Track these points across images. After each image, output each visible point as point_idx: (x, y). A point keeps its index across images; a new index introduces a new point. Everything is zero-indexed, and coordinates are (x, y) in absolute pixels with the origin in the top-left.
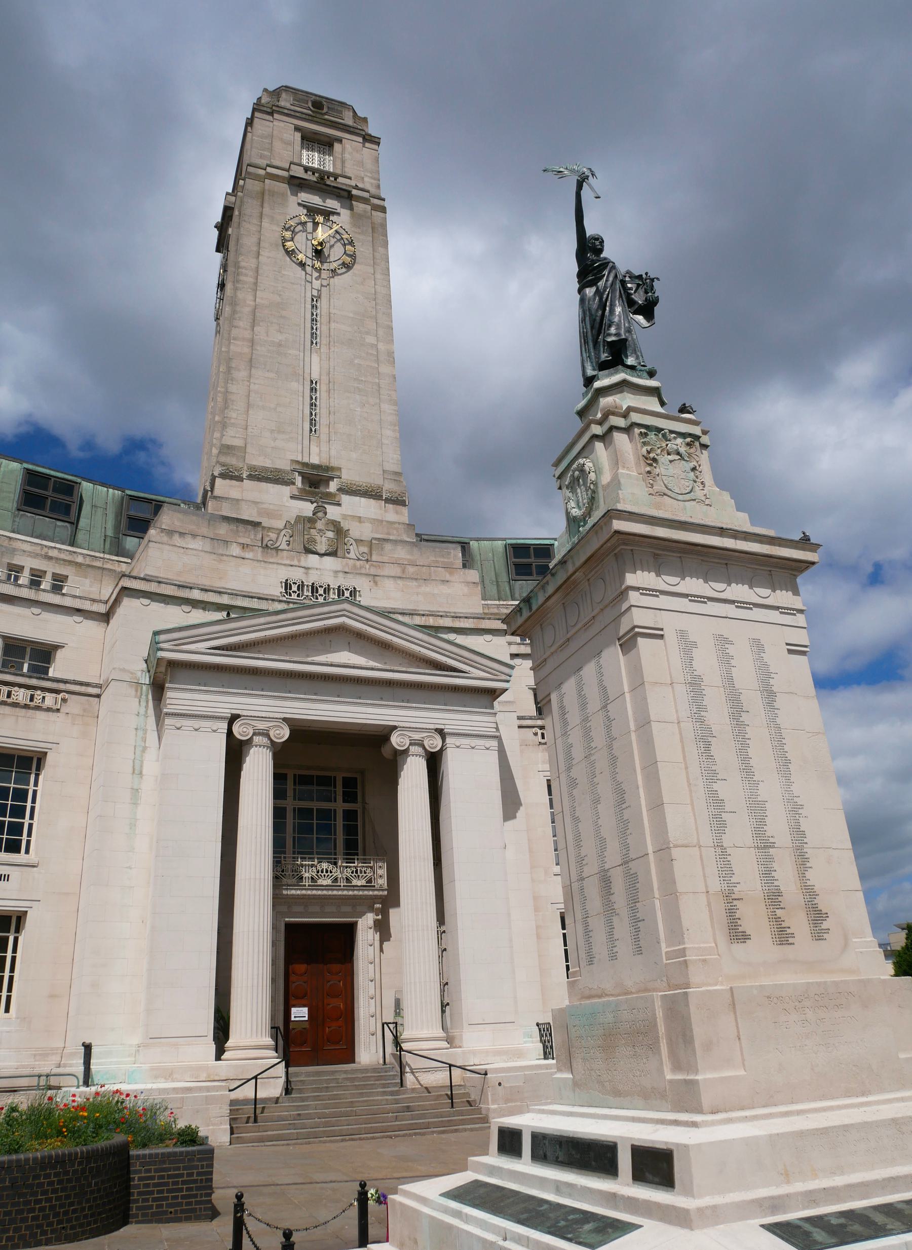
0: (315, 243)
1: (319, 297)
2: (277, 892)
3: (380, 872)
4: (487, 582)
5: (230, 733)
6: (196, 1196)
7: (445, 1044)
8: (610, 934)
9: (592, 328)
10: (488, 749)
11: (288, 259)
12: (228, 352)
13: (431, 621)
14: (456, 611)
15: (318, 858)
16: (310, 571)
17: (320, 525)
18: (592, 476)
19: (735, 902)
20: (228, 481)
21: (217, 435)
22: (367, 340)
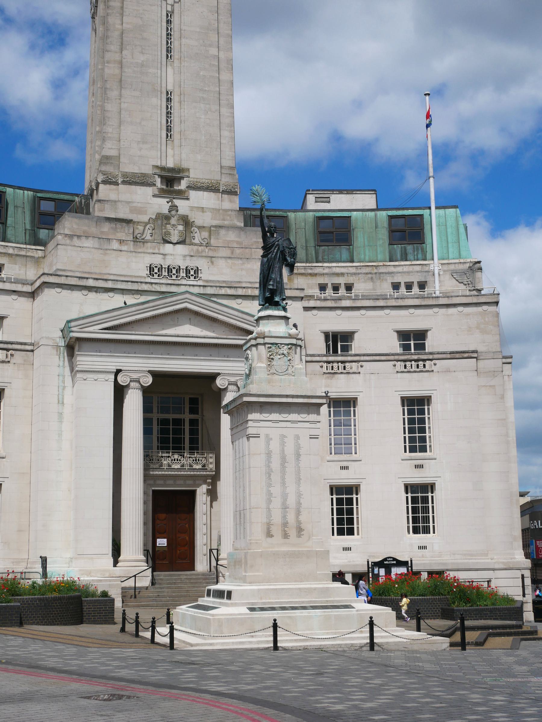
2: (147, 472)
3: (211, 460)
6: (108, 615)
15: (172, 452)
16: (167, 257)
17: (173, 221)
20: (108, 186)
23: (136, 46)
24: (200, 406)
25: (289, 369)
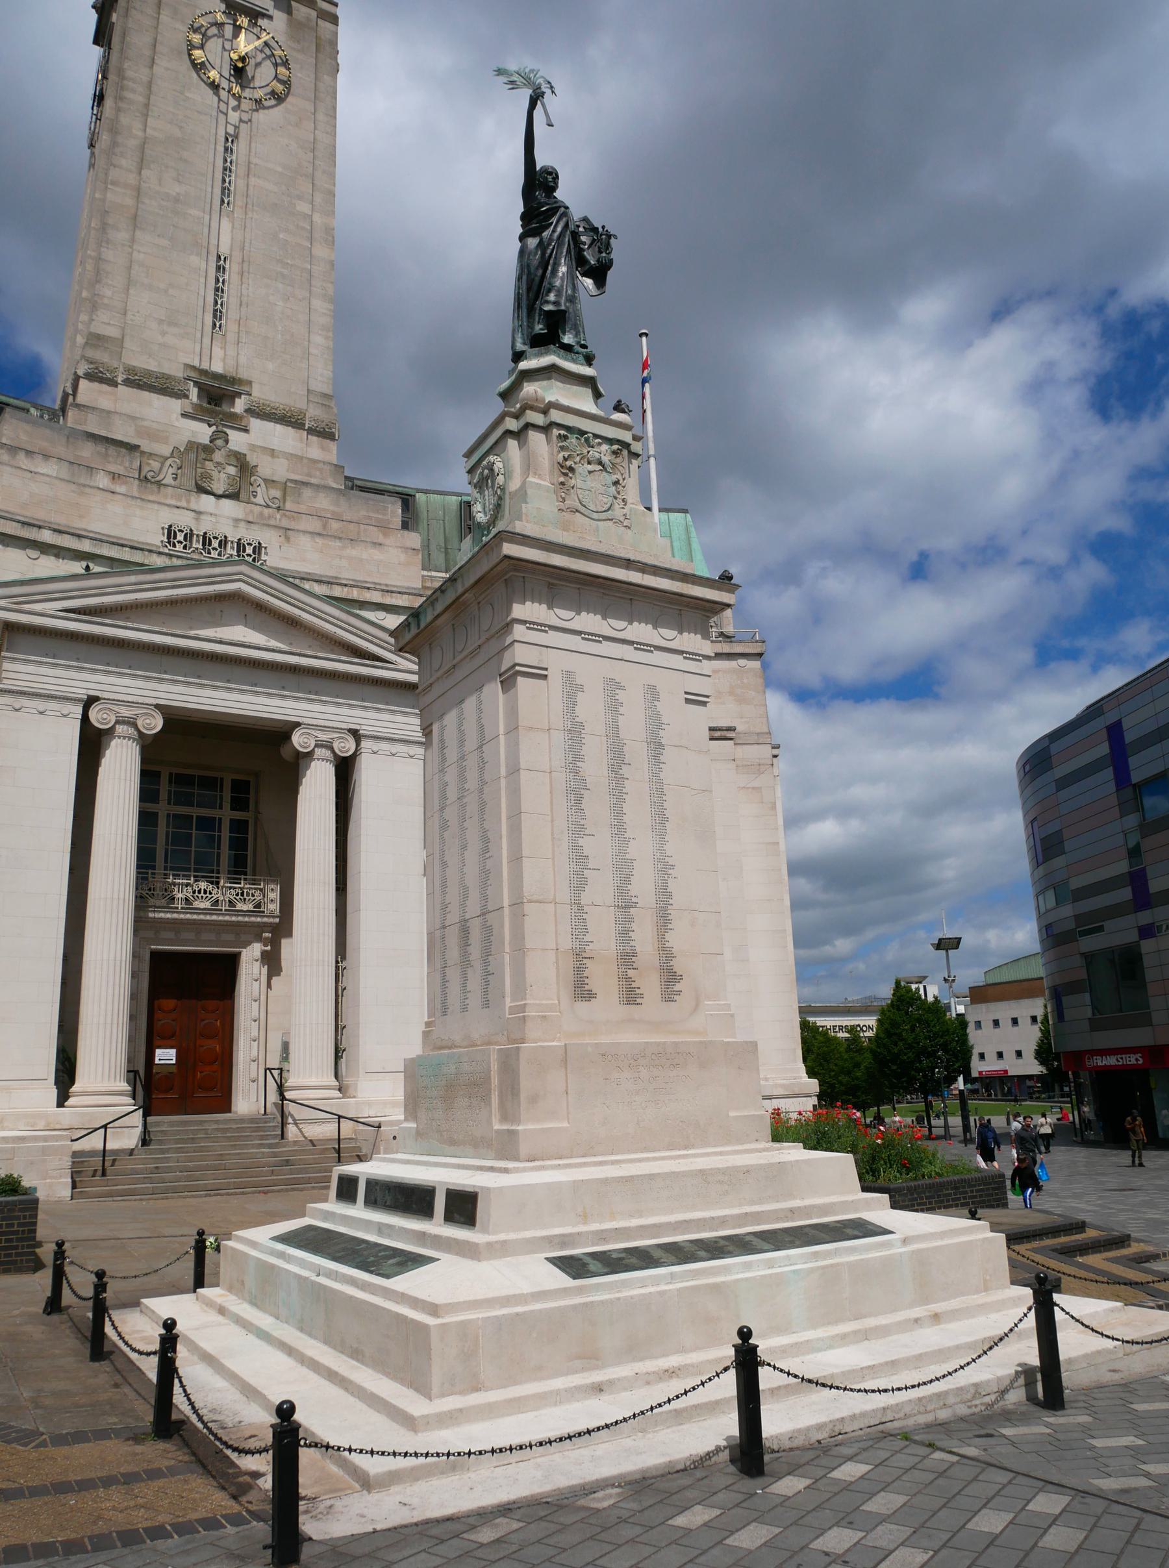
0: (235, 56)
1: (236, 136)
2: (142, 914)
3: (272, 895)
4: (433, 547)
5: (85, 719)
6: (16, 1247)
7: (337, 1094)
8: (464, 985)
9: (529, 289)
10: (412, 757)
11: (195, 75)
12: (104, 200)
13: (355, 594)
14: (389, 583)
16: (203, 517)
17: (218, 456)
18: (500, 479)
19: (585, 961)
20: (96, 384)
21: (84, 317)
22: (298, 208)
23: (167, 167)
24: (252, 796)
25: (617, 506)
